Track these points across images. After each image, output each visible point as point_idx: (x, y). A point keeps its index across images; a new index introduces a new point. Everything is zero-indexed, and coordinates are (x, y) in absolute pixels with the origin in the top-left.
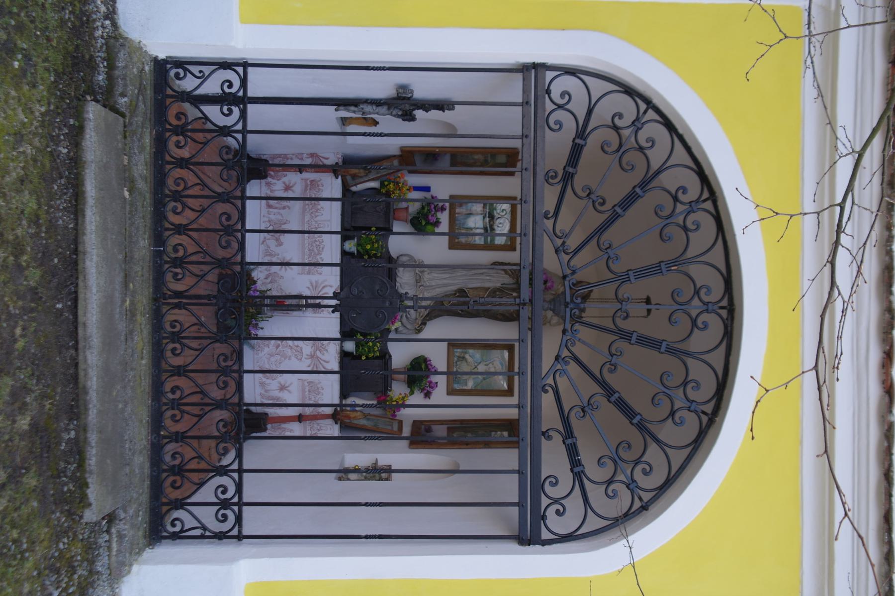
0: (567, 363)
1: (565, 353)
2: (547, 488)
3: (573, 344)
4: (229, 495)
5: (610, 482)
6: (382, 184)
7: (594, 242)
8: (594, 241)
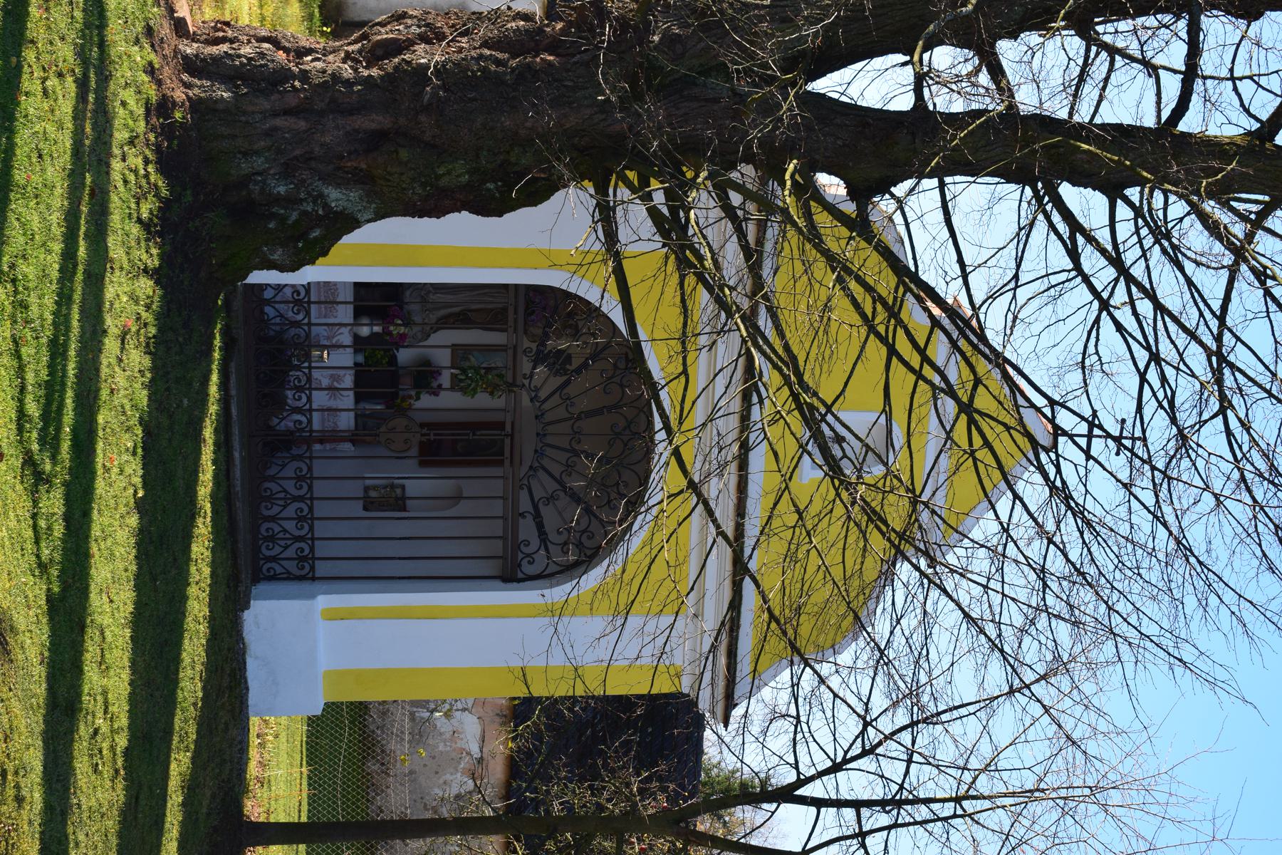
4: (303, 383)
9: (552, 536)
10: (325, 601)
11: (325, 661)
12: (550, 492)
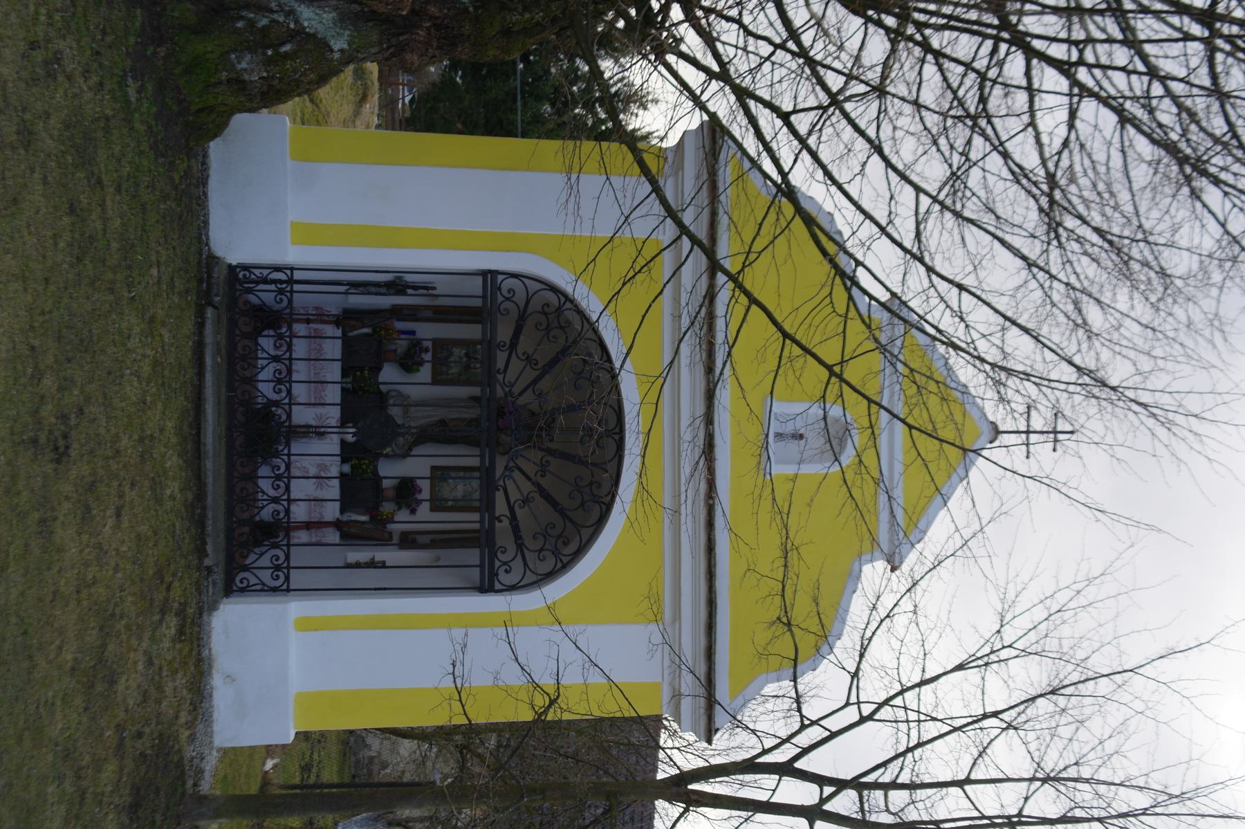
0: (513, 471)
1: (512, 464)
2: (499, 554)
3: (517, 458)
5: (541, 550)
6: (374, 331)
7: (530, 390)
8: (530, 390)
9: (528, 541)
10: (296, 608)
11: (297, 682)
12: (525, 495)
